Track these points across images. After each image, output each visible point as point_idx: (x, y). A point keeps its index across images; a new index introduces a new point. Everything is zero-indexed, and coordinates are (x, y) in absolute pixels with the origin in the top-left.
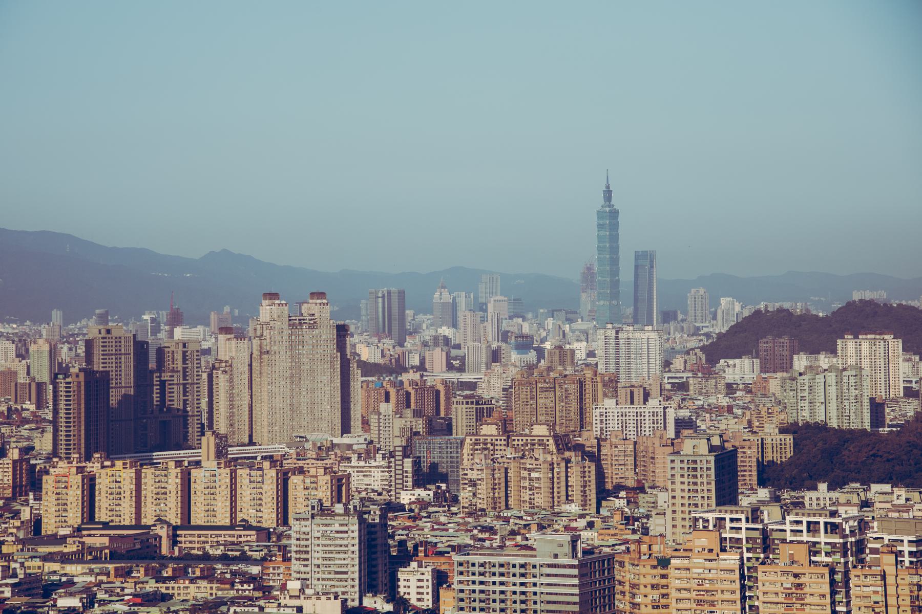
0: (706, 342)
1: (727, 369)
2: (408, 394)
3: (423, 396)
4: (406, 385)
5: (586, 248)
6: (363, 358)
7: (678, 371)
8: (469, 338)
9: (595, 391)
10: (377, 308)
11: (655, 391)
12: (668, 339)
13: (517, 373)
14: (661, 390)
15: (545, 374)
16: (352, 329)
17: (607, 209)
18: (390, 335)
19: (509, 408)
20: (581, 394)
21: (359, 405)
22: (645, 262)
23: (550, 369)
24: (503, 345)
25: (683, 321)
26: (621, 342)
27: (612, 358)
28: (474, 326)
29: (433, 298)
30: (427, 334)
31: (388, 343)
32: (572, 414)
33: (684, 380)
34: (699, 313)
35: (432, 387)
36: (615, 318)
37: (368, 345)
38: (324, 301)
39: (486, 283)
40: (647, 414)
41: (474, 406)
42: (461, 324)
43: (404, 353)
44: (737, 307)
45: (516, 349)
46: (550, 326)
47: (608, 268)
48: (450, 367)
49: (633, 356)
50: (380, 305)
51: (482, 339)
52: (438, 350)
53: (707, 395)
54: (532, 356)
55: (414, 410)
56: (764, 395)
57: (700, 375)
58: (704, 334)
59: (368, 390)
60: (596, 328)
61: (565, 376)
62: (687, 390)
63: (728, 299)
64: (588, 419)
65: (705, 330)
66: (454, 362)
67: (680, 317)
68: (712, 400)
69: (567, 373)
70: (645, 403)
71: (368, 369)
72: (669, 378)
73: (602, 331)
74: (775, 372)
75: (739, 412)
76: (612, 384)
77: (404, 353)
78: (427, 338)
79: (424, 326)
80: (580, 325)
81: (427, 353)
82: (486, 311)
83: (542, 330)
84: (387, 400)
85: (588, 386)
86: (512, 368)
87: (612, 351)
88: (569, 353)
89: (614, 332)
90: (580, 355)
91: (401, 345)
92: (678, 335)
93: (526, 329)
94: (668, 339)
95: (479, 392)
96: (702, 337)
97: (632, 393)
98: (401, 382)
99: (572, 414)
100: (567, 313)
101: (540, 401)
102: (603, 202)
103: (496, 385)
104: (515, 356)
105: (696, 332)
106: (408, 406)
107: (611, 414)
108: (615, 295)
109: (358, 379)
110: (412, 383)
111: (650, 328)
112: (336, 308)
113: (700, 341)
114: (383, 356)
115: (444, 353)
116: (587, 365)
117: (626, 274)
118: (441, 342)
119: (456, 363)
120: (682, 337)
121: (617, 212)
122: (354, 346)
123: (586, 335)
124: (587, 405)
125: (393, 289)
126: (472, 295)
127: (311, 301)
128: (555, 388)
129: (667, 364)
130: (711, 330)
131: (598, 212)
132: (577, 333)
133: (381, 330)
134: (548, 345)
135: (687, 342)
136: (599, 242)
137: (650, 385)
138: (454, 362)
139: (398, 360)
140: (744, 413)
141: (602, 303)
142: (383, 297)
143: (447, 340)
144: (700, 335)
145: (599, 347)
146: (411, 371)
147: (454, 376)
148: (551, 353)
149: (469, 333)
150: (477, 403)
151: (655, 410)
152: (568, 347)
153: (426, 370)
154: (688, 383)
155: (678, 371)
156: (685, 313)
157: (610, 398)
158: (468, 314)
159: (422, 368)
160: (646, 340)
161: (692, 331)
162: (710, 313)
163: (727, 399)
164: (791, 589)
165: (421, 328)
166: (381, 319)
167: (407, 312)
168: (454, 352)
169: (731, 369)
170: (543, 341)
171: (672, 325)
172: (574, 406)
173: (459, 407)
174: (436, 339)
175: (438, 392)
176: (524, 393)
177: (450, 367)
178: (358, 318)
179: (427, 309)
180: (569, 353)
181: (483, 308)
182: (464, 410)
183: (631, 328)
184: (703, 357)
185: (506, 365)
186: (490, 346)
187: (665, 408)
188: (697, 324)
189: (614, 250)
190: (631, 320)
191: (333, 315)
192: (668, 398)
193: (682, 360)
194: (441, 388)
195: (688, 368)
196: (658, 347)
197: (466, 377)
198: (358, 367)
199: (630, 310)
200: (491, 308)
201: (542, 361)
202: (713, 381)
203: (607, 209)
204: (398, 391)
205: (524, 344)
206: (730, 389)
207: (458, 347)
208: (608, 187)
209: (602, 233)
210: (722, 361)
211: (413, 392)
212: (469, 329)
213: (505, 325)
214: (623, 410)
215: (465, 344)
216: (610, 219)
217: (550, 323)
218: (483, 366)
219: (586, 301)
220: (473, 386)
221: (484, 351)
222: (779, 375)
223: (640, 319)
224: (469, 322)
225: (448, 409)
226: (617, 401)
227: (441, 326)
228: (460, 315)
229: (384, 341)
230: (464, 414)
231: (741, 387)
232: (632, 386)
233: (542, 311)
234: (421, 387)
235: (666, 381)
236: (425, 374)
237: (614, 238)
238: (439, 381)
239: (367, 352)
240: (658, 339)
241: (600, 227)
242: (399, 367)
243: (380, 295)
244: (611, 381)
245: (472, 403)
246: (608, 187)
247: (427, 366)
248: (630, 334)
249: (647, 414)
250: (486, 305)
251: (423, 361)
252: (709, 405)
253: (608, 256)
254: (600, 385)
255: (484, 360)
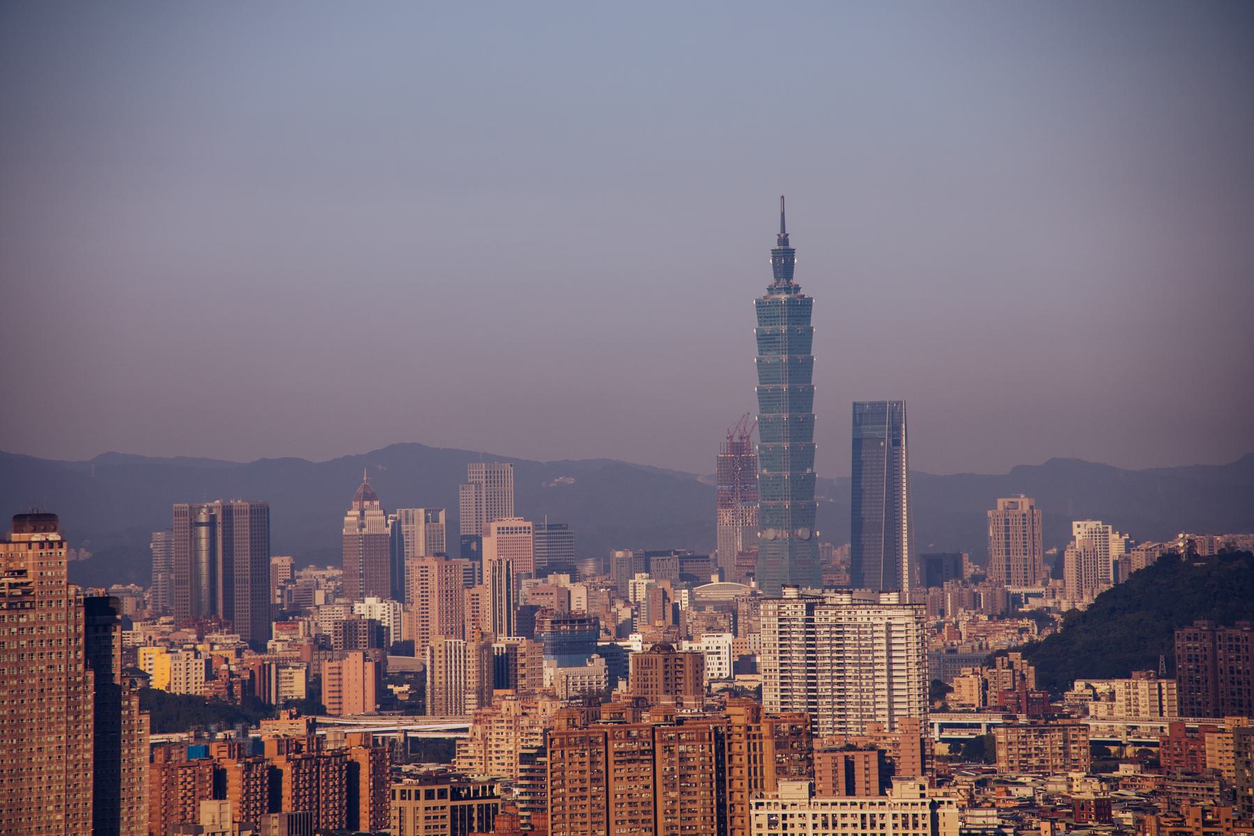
0: (1035, 634)
1: (1091, 707)
2: (275, 774)
3: (314, 781)
4: (270, 750)
5: (733, 386)
6: (158, 683)
7: (965, 708)
8: (434, 625)
9: (755, 759)
10: (195, 551)
11: (908, 759)
12: (940, 627)
13: (558, 715)
14: (923, 757)
15: (628, 716)
16: (128, 607)
17: (783, 297)
18: (228, 623)
19: (536, 806)
20: (721, 769)
21: (144, 807)
22: (877, 426)
23: (640, 704)
24: (523, 643)
25: (976, 579)
26: (822, 633)
27: (798, 674)
28: (448, 595)
29: (341, 524)
30: (327, 618)
31: (223, 644)
32: (698, 820)
33: (983, 732)
34: (1017, 558)
35: (339, 754)
36: (807, 573)
37: (171, 647)
38: (53, 537)
39: (478, 485)
40: (889, 822)
41: (448, 803)
42: (415, 590)
43: (265, 669)
44: (1116, 546)
45: (554, 652)
46: (642, 594)
47: (786, 445)
48: (386, 703)
49: (851, 671)
50: (204, 543)
51: (468, 628)
52: (355, 658)
53: (1043, 772)
54: (596, 667)
55: (290, 817)
56: (1192, 776)
57: (1023, 719)
58: (1030, 615)
59: (168, 768)
60: (756, 599)
61: (680, 721)
62: (992, 759)
63: (1092, 524)
64: (738, 821)
65: (1035, 603)
66: (396, 690)
67: (970, 569)
68: (1056, 786)
69: (685, 713)
70: (882, 793)
71: (169, 710)
72: (943, 727)
73: (772, 606)
74: (1218, 714)
75: (1128, 818)
76: (797, 745)
77: (265, 669)
78: (327, 628)
79: (319, 597)
80: (716, 589)
81: (326, 665)
82: (477, 555)
83: (619, 605)
84: (219, 792)
85: (739, 747)
86: (543, 703)
87: (798, 657)
88: (688, 662)
89: (802, 608)
90: (718, 667)
91: (259, 647)
92: (964, 617)
93: (580, 599)
94: (940, 627)
95: (461, 764)
96: (1025, 622)
97: (850, 766)
98: (258, 745)
99: (698, 820)
100: (683, 559)
101: (618, 788)
102: (771, 280)
103: (504, 747)
104: (550, 672)
105: (1010, 609)
106: (275, 806)
107: (797, 821)
108: (804, 515)
109: (142, 740)
110: (287, 745)
111: (893, 598)
112: (84, 555)
113: (1023, 630)
114: (210, 675)
115: (370, 667)
116: (736, 693)
117: (832, 459)
118: (363, 638)
119: (401, 690)
120: (974, 622)
121: (808, 303)
122: (134, 651)
123: (730, 617)
124: (737, 796)
125: (238, 503)
126: (442, 516)
127: (15, 537)
128: (653, 751)
129: (937, 691)
130: (1050, 603)
131: (760, 305)
132: (709, 610)
133: (206, 609)
134: (635, 643)
135: (988, 633)
136: (763, 380)
137: (896, 745)
138: (396, 690)
139: (248, 686)
140: (1139, 821)
141: (771, 533)
142: (212, 524)
143: (377, 632)
144: (1021, 616)
145: (764, 642)
146: (284, 715)
147: (393, 726)
148: (644, 662)
149: (434, 613)
150: (456, 795)
151: (910, 811)
152: (686, 645)
153: (322, 711)
154: (991, 739)
155: (965, 708)
156: (982, 558)
157: (793, 778)
158: (432, 563)
159: (311, 704)
160: (887, 625)
161: (1000, 606)
162: (1047, 559)
163: (1096, 785)
164: (1027, 595)
165: (311, 602)
166: (204, 581)
167: (275, 560)
168: (396, 663)
169: (1101, 708)
170: (625, 630)
171: (949, 593)
172: (703, 800)
173: (408, 805)
174: (350, 632)
175: (354, 768)
176: (575, 766)
177: (386, 703)
178: (145, 580)
179: (327, 551)
180: (688, 662)
181: (469, 548)
182: (421, 814)
183: (846, 599)
184: (1030, 673)
185: (530, 694)
186: (488, 646)
187: (934, 806)
188: (1013, 590)
189: (802, 399)
190: (845, 578)
191: (76, 573)
192: (942, 780)
193: (975, 681)
194: (362, 757)
195: (991, 702)
196: (913, 646)
197: (427, 727)
198: (141, 707)
199: (842, 553)
200: (489, 548)
201: (622, 685)
202: (1058, 735)
203: (783, 297)
204: (248, 768)
205: (576, 639)
206: (1103, 757)
207: (406, 648)
208: (784, 240)
209: (770, 358)
210: (1079, 685)
211: (287, 770)
212: (434, 603)
213: (526, 591)
214: (829, 811)
215: (425, 640)
216: (788, 320)
217: (640, 584)
218: (471, 700)
219: (732, 528)
220: (444, 750)
221: (472, 659)
222: (1229, 723)
223: (867, 574)
224: (434, 584)
225: (379, 811)
226: (812, 787)
227: (361, 597)
228: (413, 567)
229: (215, 636)
230: (422, 823)
231: (1129, 751)
232: (850, 747)
233: (619, 554)
234: (308, 755)
235: (936, 734)
236: (320, 719)
237: (801, 369)
238: (356, 740)
239: (163, 669)
240: (912, 627)
241: (765, 341)
242: (251, 703)
243: (203, 518)
244: (796, 733)
245: (442, 794)
246: (784, 240)
247: (326, 700)
248: (844, 613)
249: (889, 822)
250: (479, 540)
251: (314, 686)
252: (1047, 800)
253: (785, 416)
254: (768, 745)
255: (473, 682)
